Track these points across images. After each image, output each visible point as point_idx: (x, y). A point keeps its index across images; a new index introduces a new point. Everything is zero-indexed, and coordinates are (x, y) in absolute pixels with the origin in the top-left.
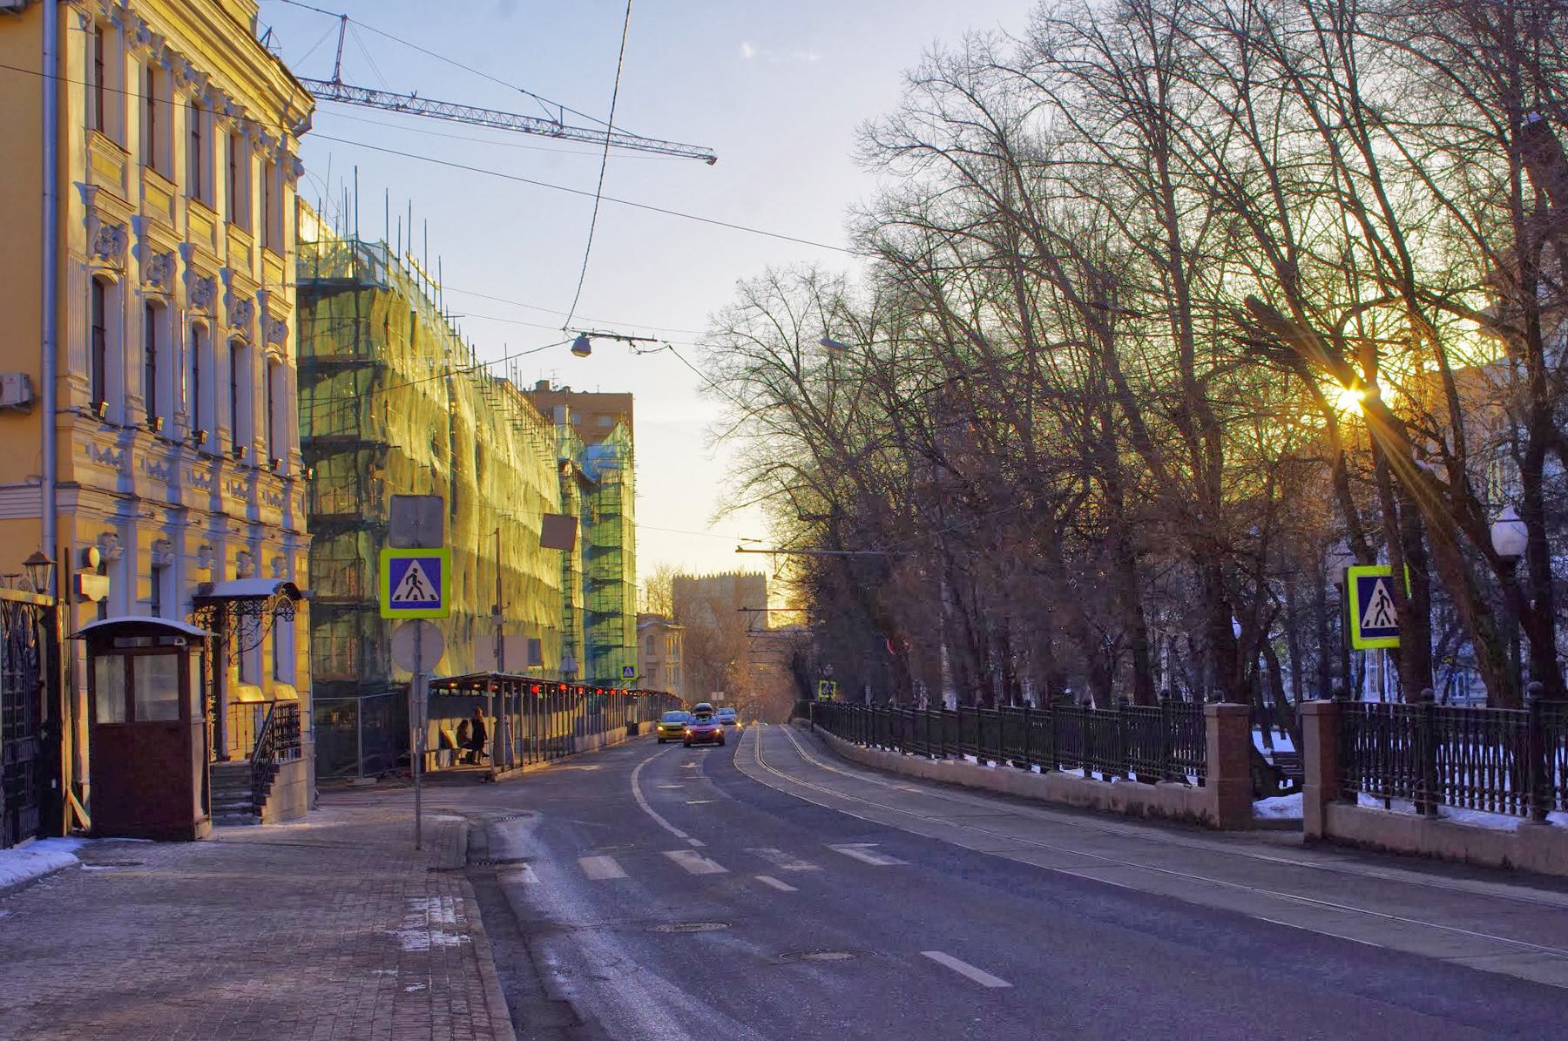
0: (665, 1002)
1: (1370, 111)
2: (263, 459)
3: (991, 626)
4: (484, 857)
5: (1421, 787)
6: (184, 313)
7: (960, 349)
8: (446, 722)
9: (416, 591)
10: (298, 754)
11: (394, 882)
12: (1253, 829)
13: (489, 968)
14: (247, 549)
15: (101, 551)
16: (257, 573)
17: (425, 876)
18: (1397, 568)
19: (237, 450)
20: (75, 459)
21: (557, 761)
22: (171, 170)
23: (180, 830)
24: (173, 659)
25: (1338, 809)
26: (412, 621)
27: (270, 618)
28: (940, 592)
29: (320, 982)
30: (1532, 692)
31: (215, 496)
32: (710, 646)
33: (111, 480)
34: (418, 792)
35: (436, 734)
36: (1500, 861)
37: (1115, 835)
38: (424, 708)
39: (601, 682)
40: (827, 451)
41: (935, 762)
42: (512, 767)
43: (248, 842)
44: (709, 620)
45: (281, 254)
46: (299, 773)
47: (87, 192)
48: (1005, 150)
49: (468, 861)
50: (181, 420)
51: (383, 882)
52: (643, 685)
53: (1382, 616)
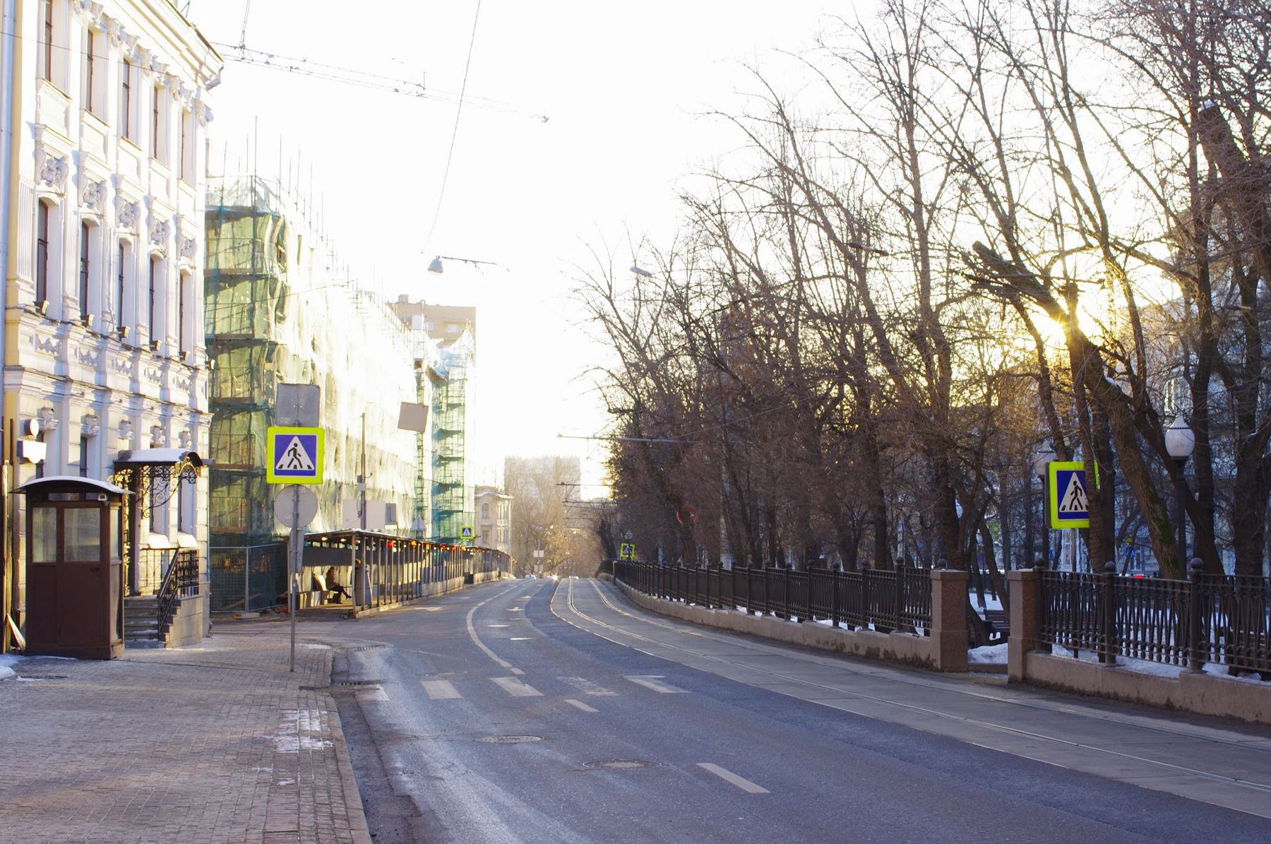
0: (488, 798)
1: (1077, 95)
2: (174, 352)
3: (761, 504)
4: (344, 678)
6: (112, 229)
7: (742, 279)
8: (317, 569)
10: (196, 591)
12: (967, 671)
13: (347, 768)
14: (159, 424)
15: (41, 421)
16: (167, 444)
17: (296, 693)
18: (1089, 463)
19: (153, 344)
20: (20, 346)
21: (407, 602)
22: (105, 114)
23: (102, 652)
24: (96, 512)
25: (1036, 658)
26: (293, 486)
27: (177, 481)
28: (720, 475)
29: (209, 775)
31: (134, 380)
33: (49, 365)
34: (293, 626)
35: (307, 579)
37: (856, 674)
38: (300, 558)
40: (633, 357)
41: (713, 611)
43: (153, 662)
44: (533, 492)
45: (192, 184)
46: (195, 608)
47: (36, 130)
50: (108, 317)
51: (263, 697)
52: (478, 544)
53: (1076, 502)
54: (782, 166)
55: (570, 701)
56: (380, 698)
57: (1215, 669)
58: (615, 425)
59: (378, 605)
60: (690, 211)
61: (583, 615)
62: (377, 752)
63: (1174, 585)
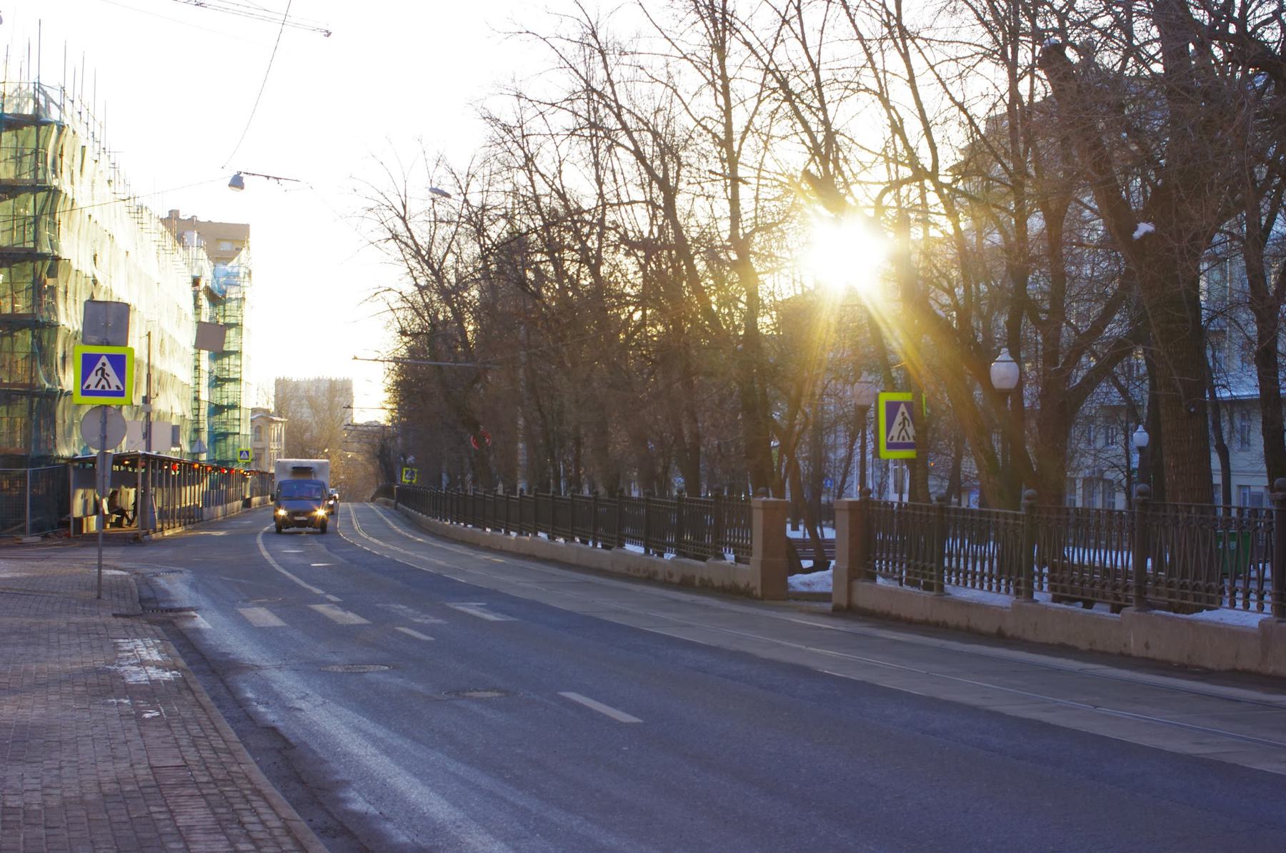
0: (357, 729)
4: (154, 605)
5: (931, 570)
7: (545, 200)
9: (103, 382)
11: (96, 625)
13: (206, 699)
17: (113, 620)
21: (189, 527)
25: (861, 586)
29: (66, 708)
30: (1028, 498)
32: (308, 434)
34: (100, 552)
36: (994, 630)
37: (677, 601)
38: (108, 481)
42: (155, 531)
44: (306, 414)
48: (595, 44)
49: (143, 608)
53: (903, 433)
54: (590, 90)
55: (402, 629)
57: (1043, 596)
58: (394, 345)
59: (162, 530)
60: (488, 131)
61: (376, 541)
62: (222, 681)
63: (1006, 516)
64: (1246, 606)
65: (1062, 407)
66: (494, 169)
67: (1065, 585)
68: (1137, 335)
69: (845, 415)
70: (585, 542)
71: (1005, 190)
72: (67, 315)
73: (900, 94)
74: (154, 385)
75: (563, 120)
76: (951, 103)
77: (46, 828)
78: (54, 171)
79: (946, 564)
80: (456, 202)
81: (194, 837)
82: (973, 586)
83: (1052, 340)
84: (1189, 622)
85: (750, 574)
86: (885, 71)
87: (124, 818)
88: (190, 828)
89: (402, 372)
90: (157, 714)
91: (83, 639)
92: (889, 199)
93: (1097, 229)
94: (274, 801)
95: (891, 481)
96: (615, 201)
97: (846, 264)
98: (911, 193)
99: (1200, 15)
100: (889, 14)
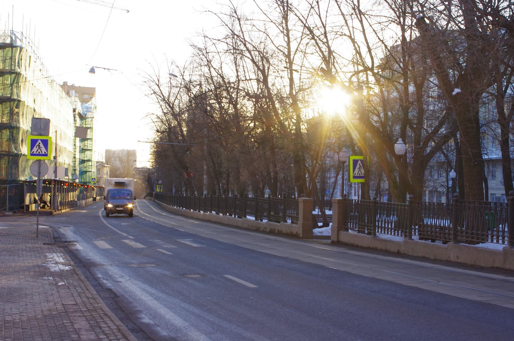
0: (144, 290)
5: (371, 227)
9: (39, 150)
11: (37, 248)
12: (313, 238)
13: (83, 277)
21: (72, 209)
25: (343, 233)
26: (37, 160)
29: (28, 281)
34: (38, 218)
36: (396, 251)
37: (269, 239)
38: (41, 190)
39: (84, 183)
44: (118, 164)
51: (33, 248)
53: (360, 172)
56: (79, 248)
57: (415, 237)
58: (154, 136)
59: (61, 210)
60: (192, 50)
64: (498, 242)
65: (422, 162)
66: (195, 66)
67: (425, 233)
68: (452, 134)
69: (333, 166)
70: (231, 215)
71: (399, 75)
72: (23, 124)
73: (359, 37)
74: (58, 152)
75: (223, 47)
76: (379, 40)
77: (23, 329)
78: (19, 66)
79: (377, 224)
80: (180, 78)
81: (82, 333)
82: (388, 233)
83: (418, 136)
84: (475, 248)
85: (298, 228)
86: (353, 28)
87: (54, 325)
88: (80, 329)
89: (157, 147)
90: (64, 283)
91: (32, 253)
92: (354, 79)
93: (434, 92)
94: (113, 318)
95: (353, 191)
96: (244, 79)
97: (333, 105)
98: (362, 77)
99: (481, 6)
100: (354, 5)
